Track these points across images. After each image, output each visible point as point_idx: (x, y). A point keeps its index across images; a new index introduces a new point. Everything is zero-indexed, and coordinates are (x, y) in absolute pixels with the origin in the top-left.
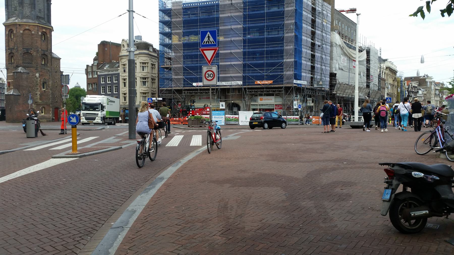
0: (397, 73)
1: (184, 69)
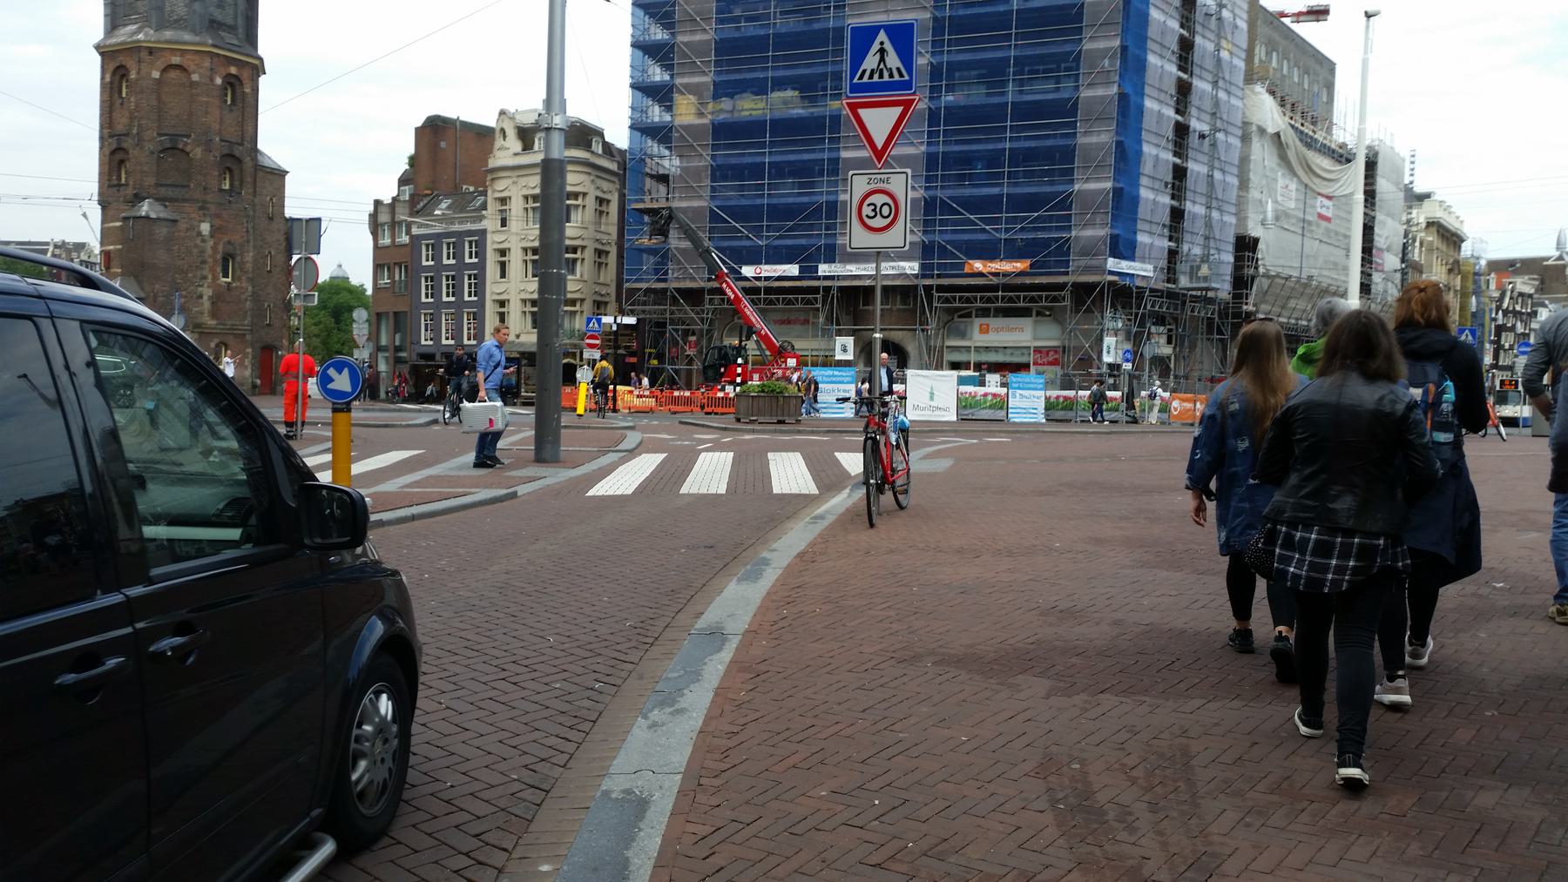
1: (714, 217)
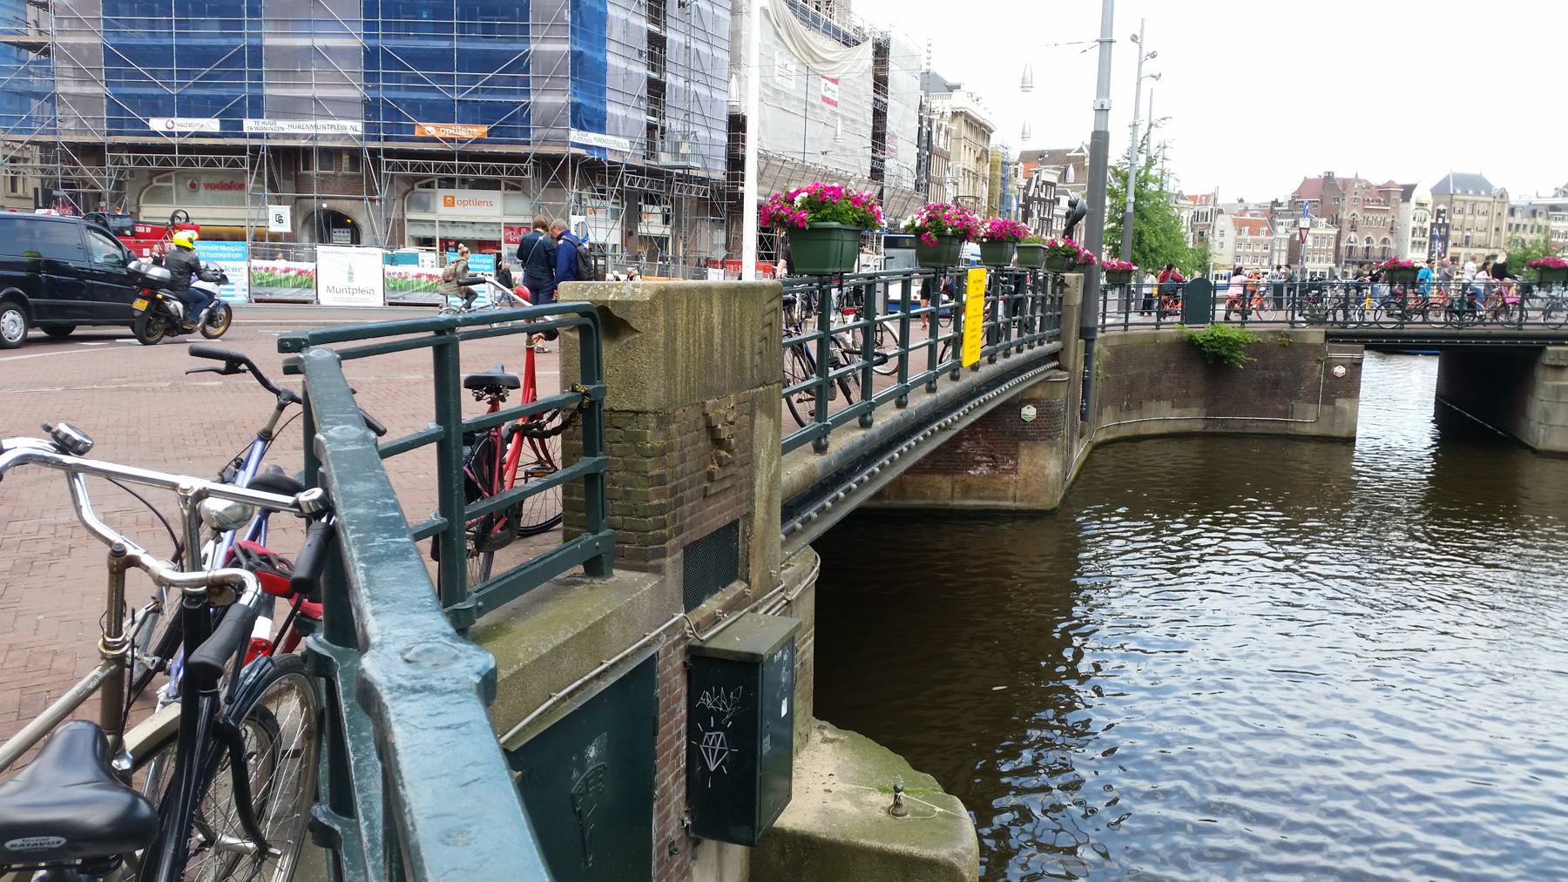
0: (992, 135)
1: (110, 57)
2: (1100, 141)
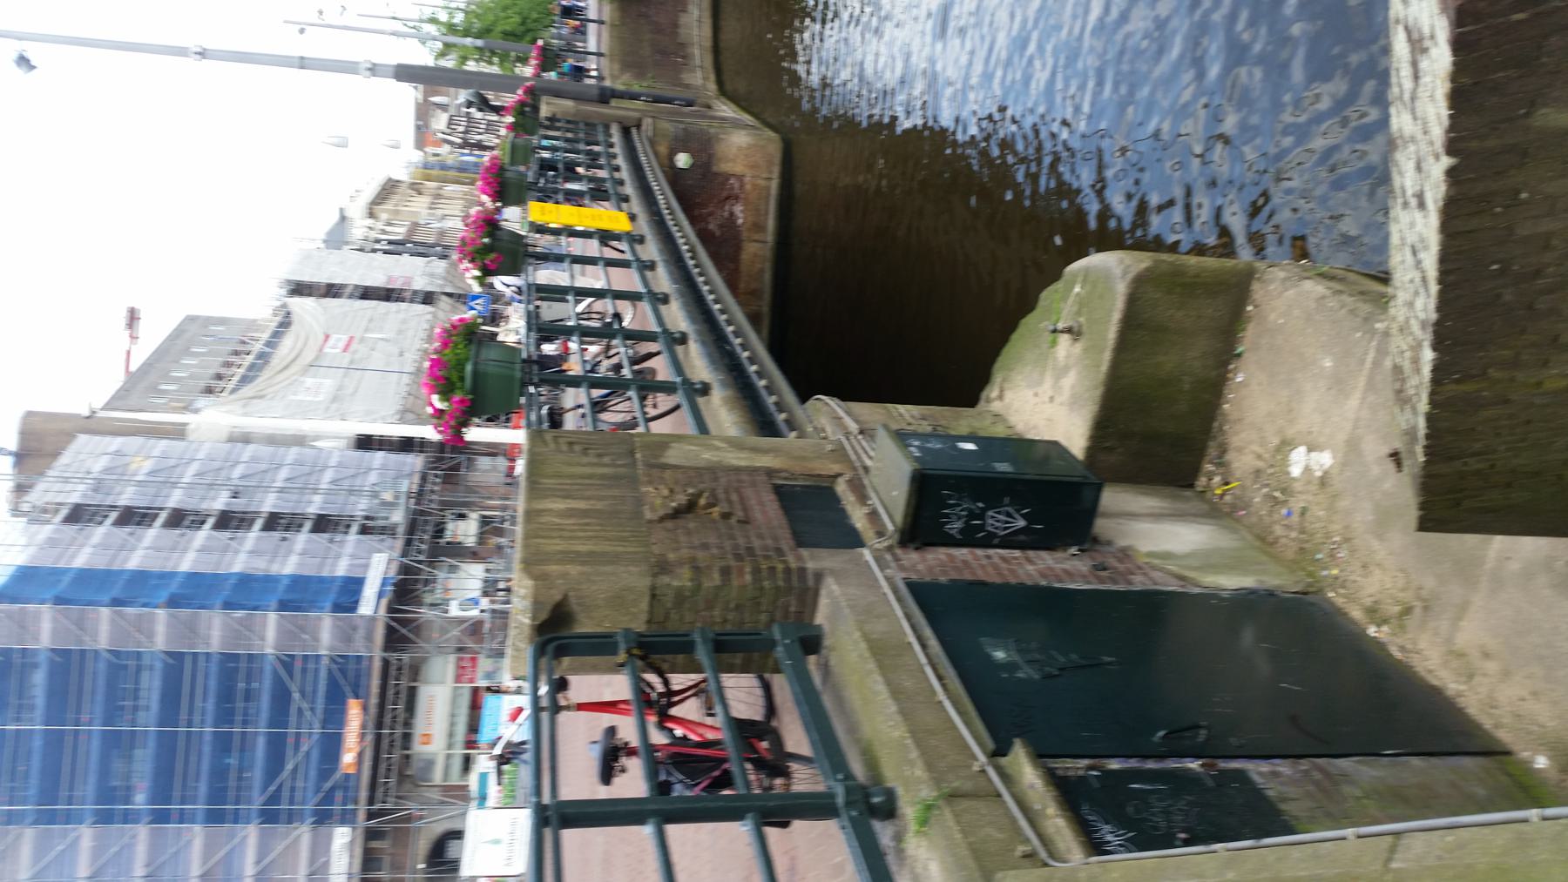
2: (405, 73)
